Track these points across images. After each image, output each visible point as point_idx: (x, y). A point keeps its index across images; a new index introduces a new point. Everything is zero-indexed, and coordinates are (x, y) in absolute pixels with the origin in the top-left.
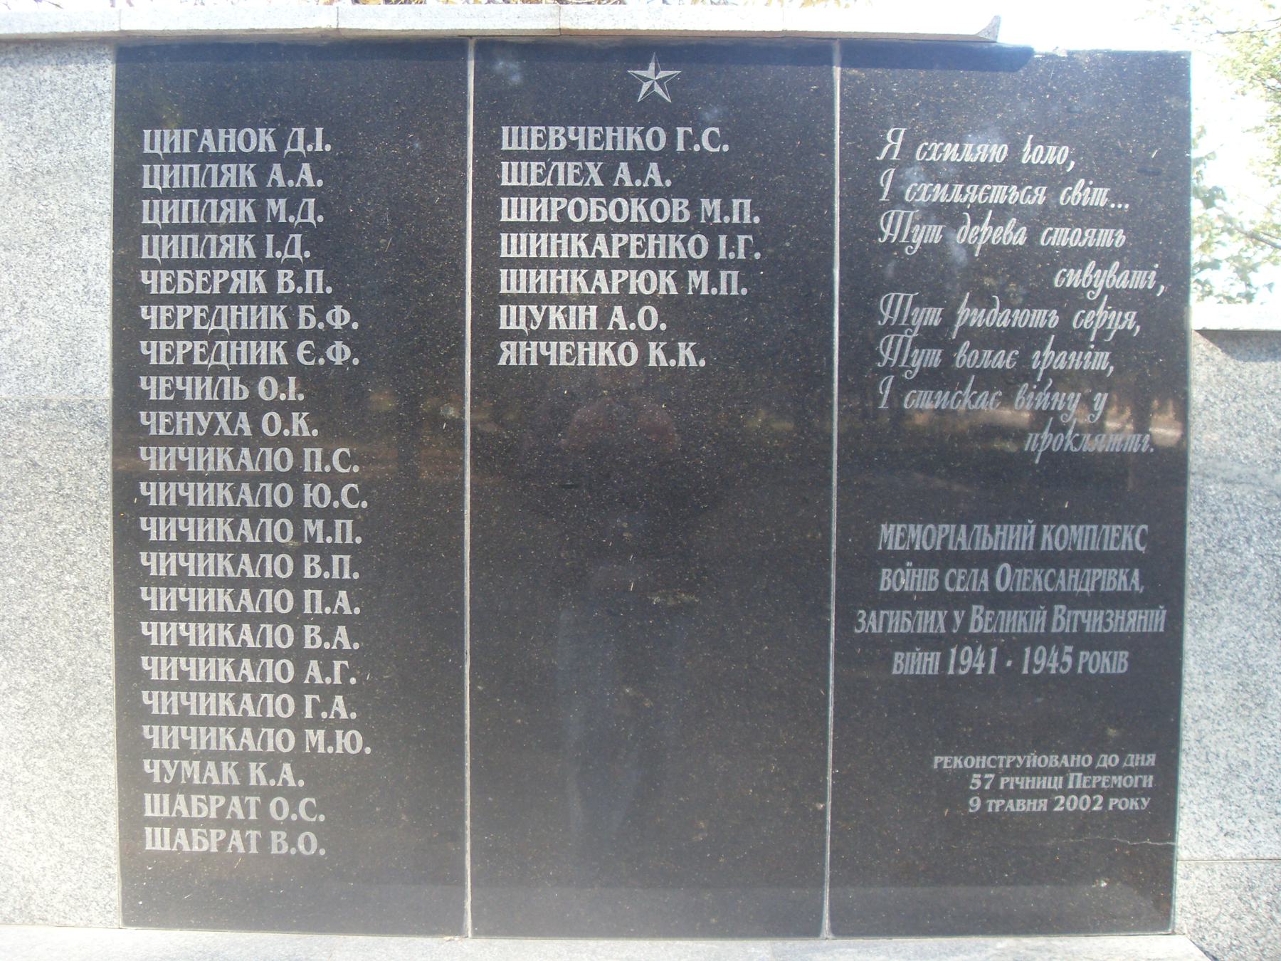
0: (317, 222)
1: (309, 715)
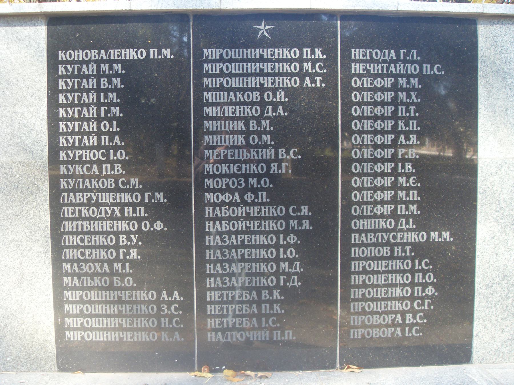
0: (298, 285)
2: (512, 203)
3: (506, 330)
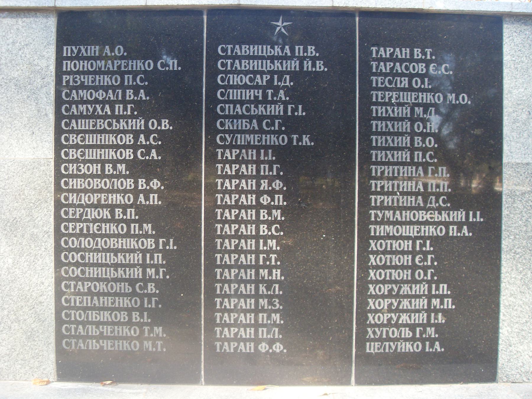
1: (261, 263)
2: (4, 206)
3: (4, 344)
